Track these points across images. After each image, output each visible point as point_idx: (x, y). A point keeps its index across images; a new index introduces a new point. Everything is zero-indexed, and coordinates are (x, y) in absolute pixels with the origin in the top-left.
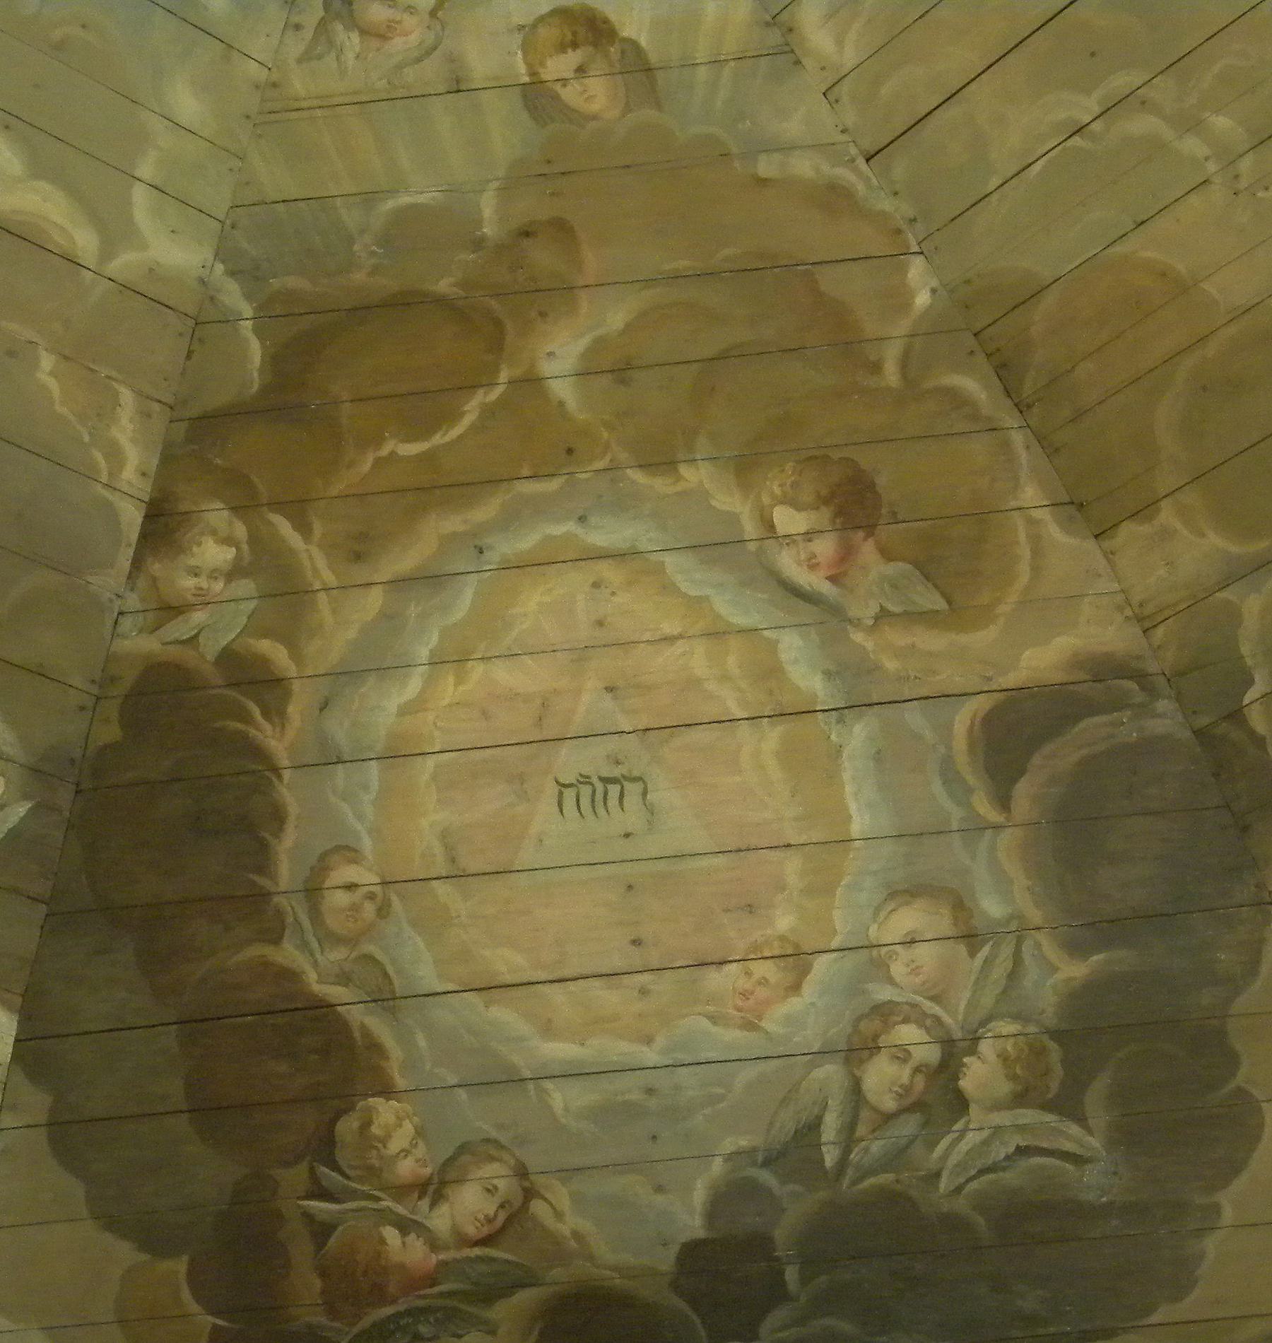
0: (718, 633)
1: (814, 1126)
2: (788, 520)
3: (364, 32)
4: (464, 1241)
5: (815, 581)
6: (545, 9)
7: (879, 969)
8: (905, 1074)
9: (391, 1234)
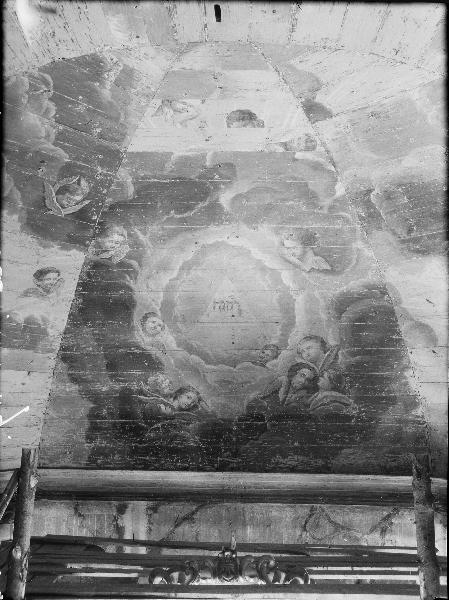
0: (263, 269)
4: (181, 409)
5: (294, 260)
6: (235, 109)
9: (163, 407)
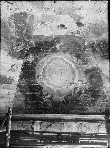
1: (71, 94)
2: (73, 57)
3: (44, 25)
4: (48, 99)
7: (77, 84)
8: (78, 91)
9: (43, 98)
